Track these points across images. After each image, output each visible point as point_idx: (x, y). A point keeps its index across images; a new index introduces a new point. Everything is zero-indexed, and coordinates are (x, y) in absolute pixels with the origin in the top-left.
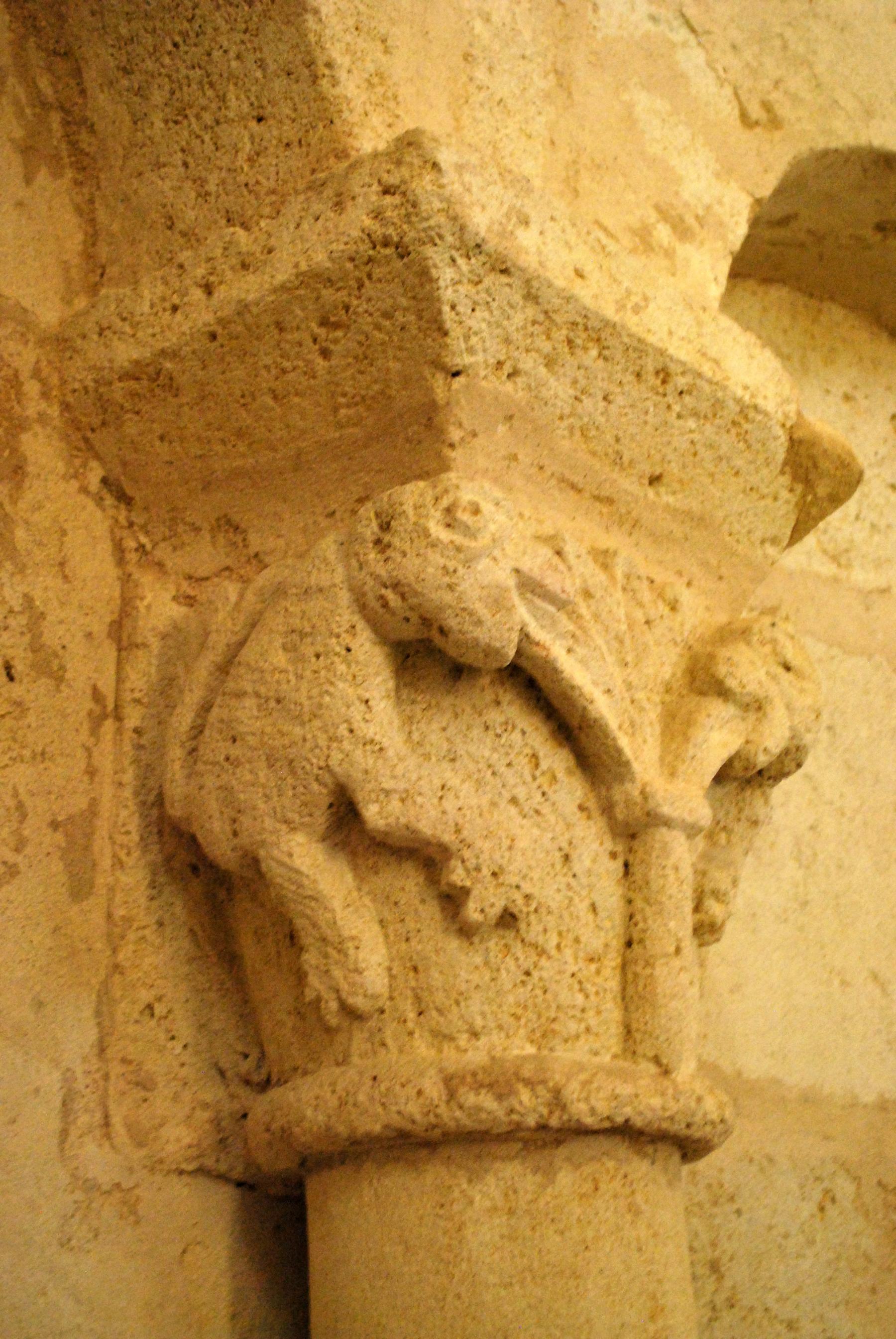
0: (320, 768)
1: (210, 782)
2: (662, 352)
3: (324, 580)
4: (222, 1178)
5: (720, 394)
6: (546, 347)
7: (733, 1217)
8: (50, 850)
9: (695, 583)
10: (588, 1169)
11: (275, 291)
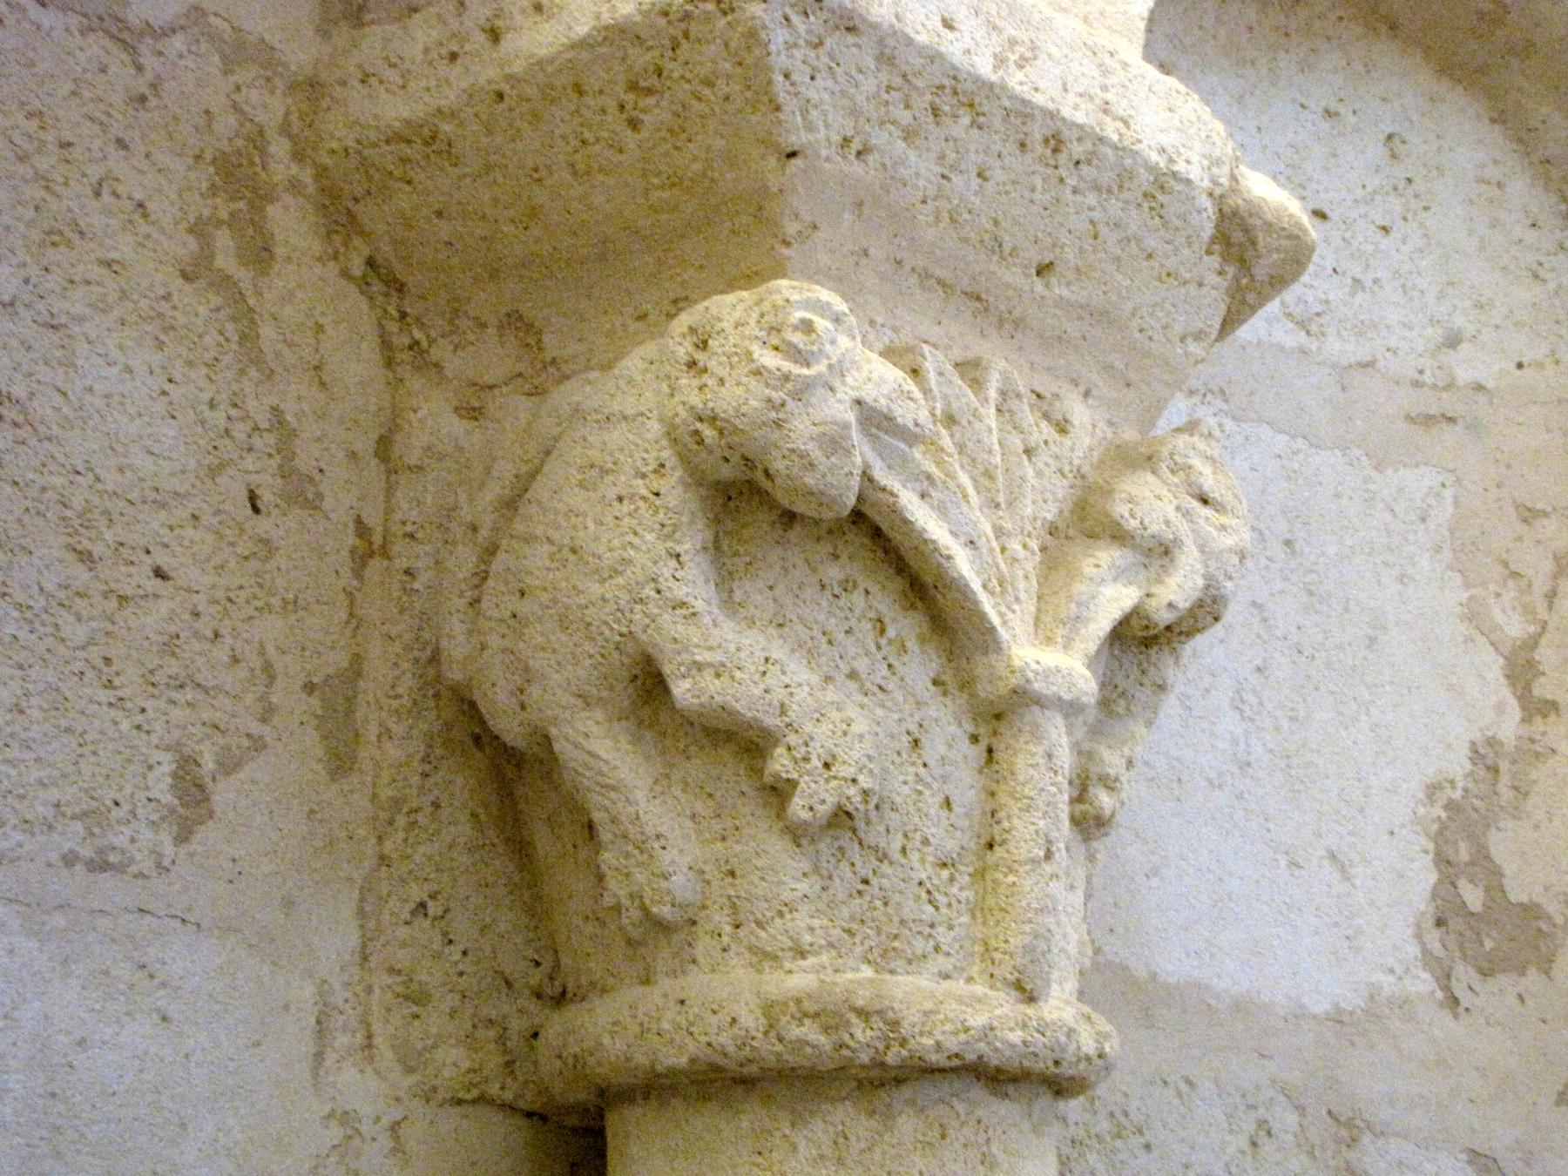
0: (621, 635)
1: (494, 641)
2: (1053, 115)
3: (629, 405)
4: (510, 1108)
5: (1128, 162)
6: (905, 117)
7: (1141, 1152)
8: (305, 718)
9: (1095, 392)
10: (933, 1113)
11: (573, 46)
